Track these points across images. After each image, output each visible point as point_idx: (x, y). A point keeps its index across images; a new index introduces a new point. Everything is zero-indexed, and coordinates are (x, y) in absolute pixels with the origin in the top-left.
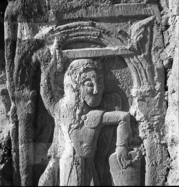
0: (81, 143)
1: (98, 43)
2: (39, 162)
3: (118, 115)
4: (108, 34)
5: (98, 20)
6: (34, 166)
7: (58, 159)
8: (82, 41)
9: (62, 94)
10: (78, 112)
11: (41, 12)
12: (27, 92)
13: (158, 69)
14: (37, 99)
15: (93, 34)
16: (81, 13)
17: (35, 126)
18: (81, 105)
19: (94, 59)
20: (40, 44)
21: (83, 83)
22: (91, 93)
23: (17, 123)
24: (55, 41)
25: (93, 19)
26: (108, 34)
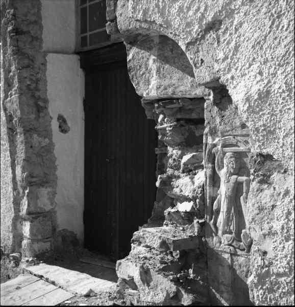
0: (229, 189)
1: (236, 145)
2: (215, 196)
3: (244, 178)
4: (240, 142)
5: (237, 136)
6: (212, 198)
7: (221, 196)
8: (231, 144)
9: (223, 167)
10: (228, 175)
11: (216, 133)
12: (210, 165)
13: (27, 266)
14: (214, 168)
15: (234, 141)
16: (230, 132)
17: (213, 180)
18: (229, 172)
19: (235, 152)
20: (215, 146)
21: (230, 163)
22: (233, 168)
23: (206, 178)
24: (221, 144)
25: (235, 135)
26: (240, 142)
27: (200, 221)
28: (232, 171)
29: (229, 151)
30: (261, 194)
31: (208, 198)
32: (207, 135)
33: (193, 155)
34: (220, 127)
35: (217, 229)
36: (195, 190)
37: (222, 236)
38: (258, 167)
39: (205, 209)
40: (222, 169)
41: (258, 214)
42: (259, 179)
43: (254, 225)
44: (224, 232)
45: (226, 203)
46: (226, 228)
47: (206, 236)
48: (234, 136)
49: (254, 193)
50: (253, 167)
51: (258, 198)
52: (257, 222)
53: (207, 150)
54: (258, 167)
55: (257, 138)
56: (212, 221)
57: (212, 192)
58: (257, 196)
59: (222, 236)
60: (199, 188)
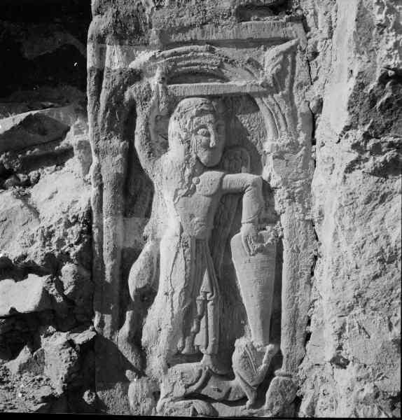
0: (192, 216)
1: (218, 75)
2: (130, 245)
3: (244, 178)
9: (165, 146)
10: (188, 172)
11: (138, 32)
12: (117, 143)
17: (126, 192)
18: (193, 162)
21: (195, 132)
22: (206, 146)
23: (101, 187)
25: (212, 43)
27: (80, 339)
28: (204, 158)
29: (191, 98)
30: (380, 209)
31: (106, 254)
32: (101, 39)
33: (28, 118)
34: (158, 14)
35: (141, 352)
36: (51, 235)
37: (166, 372)
38: (382, 121)
39: (97, 295)
40: (161, 154)
41: (376, 277)
42: (381, 159)
43: (362, 317)
44: (174, 358)
45: (181, 264)
46: (180, 344)
47: (98, 385)
48: (212, 45)
49: (358, 211)
50: (361, 121)
51: (373, 224)
52: (373, 303)
53: (104, 94)
54: (382, 121)
55: (392, 17)
56: (126, 328)
57: (120, 233)
58: (369, 219)
59: (166, 372)
60: (68, 225)
